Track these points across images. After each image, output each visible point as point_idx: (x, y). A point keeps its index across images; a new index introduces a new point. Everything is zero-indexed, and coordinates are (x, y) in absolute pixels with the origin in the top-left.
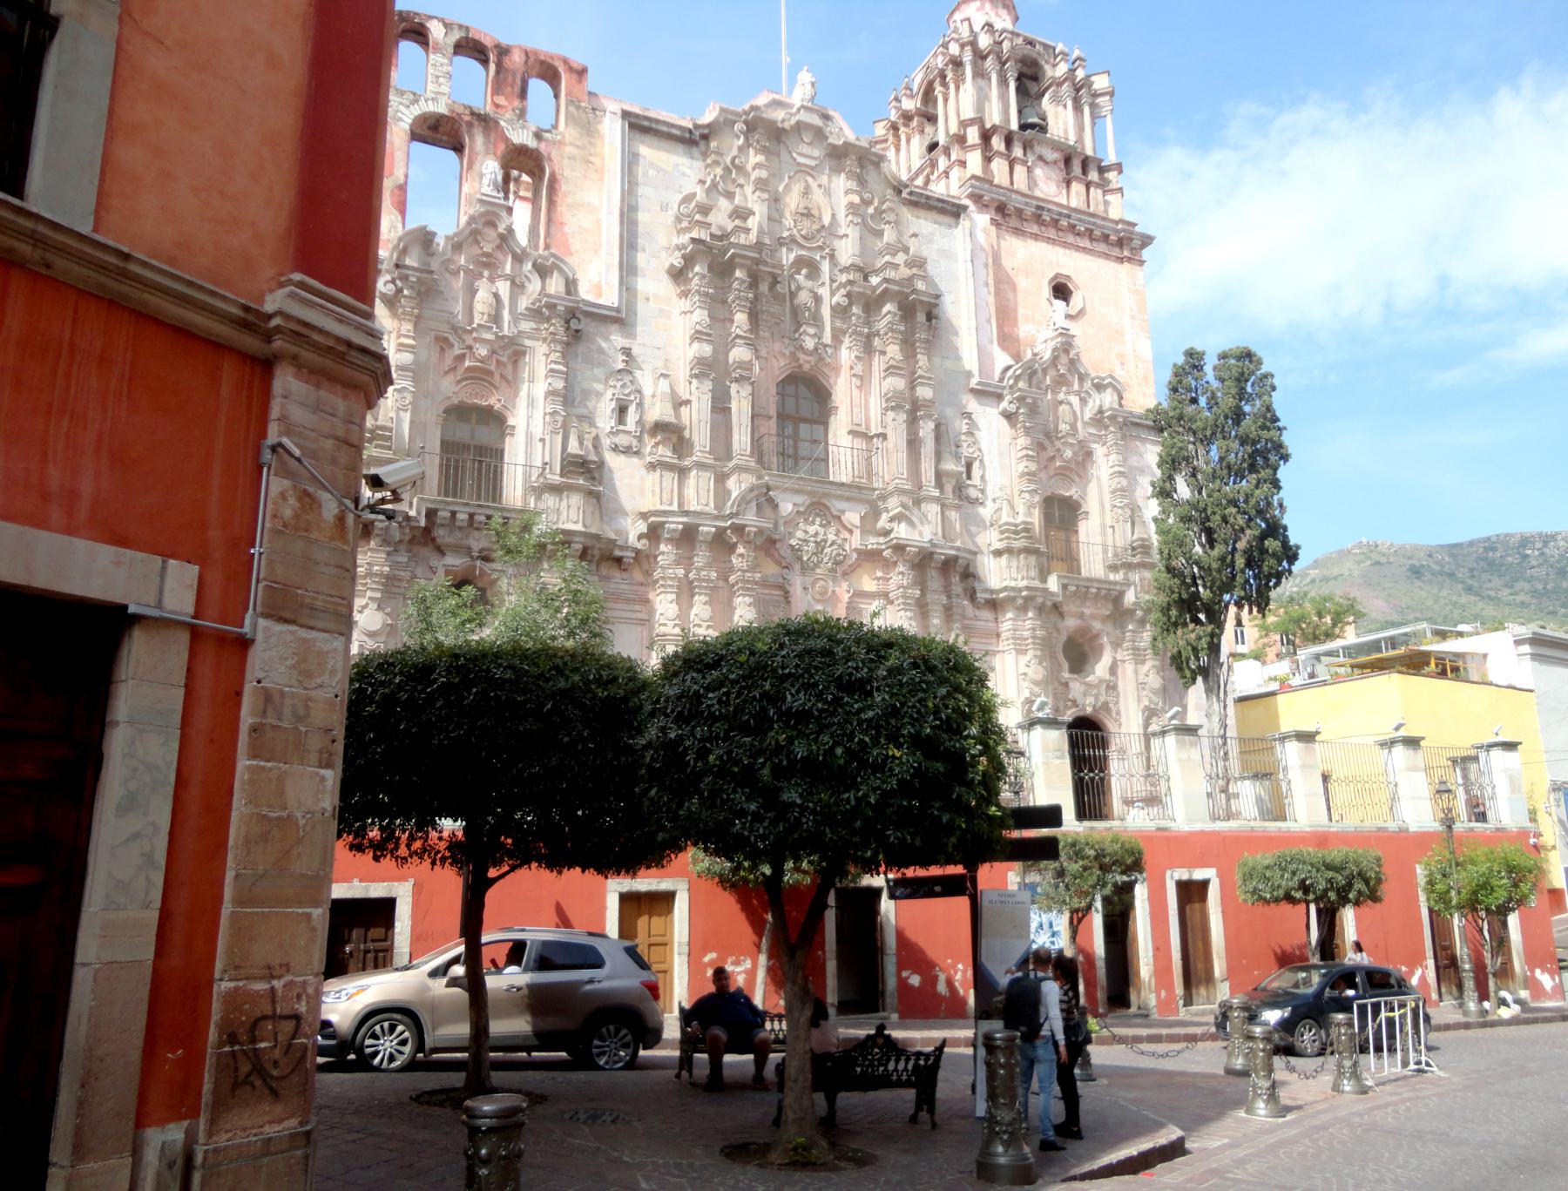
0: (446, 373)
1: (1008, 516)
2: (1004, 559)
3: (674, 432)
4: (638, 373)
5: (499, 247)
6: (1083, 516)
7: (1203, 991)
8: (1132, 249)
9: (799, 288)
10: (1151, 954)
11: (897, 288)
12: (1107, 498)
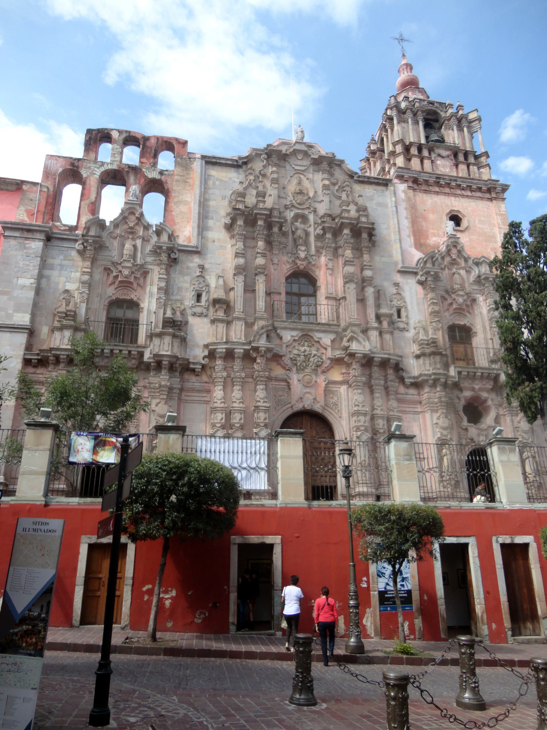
0: (110, 285)
1: (423, 336)
2: (421, 360)
3: (224, 303)
4: (207, 277)
5: (137, 224)
6: (474, 334)
7: (529, 625)
8: (497, 193)
9: (297, 229)
10: (482, 596)
11: (348, 221)
12: (487, 324)
